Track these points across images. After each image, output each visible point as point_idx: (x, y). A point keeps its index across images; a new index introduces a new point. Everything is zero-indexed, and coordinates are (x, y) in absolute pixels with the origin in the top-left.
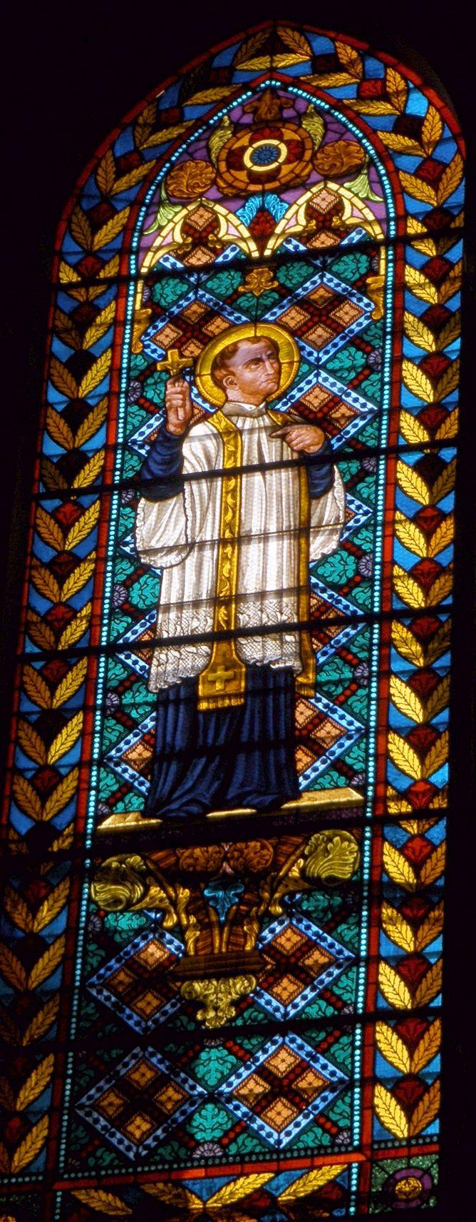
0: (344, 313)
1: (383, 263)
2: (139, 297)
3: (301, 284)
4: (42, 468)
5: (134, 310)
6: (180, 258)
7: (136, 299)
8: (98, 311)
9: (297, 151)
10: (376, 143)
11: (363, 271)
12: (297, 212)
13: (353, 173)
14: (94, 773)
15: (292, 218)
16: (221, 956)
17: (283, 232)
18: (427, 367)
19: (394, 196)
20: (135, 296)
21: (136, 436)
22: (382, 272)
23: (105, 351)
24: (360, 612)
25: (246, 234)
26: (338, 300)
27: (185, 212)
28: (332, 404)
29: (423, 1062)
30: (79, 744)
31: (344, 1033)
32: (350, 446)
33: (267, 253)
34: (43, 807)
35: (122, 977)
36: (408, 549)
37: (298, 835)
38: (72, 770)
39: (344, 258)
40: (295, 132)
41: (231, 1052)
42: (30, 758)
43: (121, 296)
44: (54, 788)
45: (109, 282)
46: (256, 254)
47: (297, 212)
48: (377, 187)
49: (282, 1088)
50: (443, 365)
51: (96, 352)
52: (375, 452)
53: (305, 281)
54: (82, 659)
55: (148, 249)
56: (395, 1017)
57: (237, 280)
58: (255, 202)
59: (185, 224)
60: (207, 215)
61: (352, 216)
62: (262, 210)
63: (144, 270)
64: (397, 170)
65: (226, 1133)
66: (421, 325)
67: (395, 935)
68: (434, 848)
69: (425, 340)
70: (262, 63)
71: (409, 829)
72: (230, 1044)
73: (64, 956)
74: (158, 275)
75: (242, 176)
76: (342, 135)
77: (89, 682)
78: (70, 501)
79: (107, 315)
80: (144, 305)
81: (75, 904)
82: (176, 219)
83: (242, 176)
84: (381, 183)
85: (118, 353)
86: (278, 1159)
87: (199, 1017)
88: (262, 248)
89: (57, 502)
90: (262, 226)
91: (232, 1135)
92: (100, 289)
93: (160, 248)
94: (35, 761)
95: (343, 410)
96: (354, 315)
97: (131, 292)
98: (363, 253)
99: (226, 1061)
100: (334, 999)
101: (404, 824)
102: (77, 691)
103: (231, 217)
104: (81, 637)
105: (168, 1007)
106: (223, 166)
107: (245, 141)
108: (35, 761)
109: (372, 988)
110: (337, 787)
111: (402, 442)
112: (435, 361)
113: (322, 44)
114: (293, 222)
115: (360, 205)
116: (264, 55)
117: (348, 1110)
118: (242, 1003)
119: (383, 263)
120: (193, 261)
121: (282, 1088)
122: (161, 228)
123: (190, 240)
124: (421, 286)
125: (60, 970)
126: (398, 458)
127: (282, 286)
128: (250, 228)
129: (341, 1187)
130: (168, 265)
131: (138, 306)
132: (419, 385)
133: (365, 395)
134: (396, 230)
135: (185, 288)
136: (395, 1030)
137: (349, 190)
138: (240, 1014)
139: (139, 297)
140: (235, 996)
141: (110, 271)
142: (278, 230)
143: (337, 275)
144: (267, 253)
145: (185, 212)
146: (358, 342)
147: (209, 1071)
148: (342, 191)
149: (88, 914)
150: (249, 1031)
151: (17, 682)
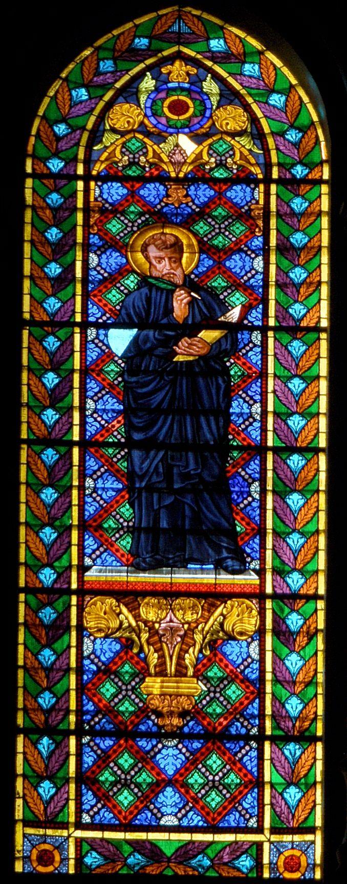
33: (181, 175)
39: (234, 187)
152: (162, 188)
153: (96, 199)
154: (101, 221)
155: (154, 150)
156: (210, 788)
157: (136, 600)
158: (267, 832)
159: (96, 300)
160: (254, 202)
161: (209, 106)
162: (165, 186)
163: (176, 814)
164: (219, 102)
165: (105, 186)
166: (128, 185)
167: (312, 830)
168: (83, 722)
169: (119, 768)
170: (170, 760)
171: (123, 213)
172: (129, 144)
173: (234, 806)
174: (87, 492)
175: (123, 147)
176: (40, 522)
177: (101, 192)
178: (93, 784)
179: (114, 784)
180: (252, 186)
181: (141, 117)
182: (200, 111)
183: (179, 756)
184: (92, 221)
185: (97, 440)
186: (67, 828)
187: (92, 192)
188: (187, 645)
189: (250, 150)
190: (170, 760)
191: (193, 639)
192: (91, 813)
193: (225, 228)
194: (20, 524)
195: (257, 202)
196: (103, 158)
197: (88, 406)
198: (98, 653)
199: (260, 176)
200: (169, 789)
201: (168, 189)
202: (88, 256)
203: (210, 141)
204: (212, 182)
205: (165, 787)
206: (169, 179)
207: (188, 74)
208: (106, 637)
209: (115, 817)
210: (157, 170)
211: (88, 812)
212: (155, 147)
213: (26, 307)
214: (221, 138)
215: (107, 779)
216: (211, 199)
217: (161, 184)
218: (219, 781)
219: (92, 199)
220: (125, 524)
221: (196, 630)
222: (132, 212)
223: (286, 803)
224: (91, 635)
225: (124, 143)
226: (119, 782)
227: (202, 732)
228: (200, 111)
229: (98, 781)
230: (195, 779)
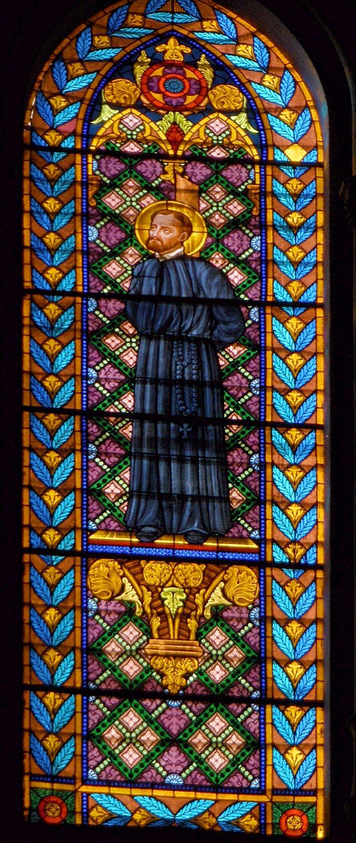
17: (190, 141)
24: (252, 419)
25: (164, 138)
27: (120, 115)
33: (179, 153)
34: (52, 477)
38: (70, 379)
39: (230, 167)
42: (40, 597)
46: (171, 152)
55: (95, 136)
61: (237, 139)
82: (114, 119)
94: (43, 600)
108: (43, 600)
114: (195, 136)
115: (243, 134)
122: (103, 123)
128: (167, 135)
135: (123, 166)
137: (234, 121)
144: (179, 153)
145: (120, 115)
148: (229, 121)
152: (158, 164)
153: (94, 173)
154: (99, 195)
155: (151, 128)
156: (214, 749)
157: (139, 565)
158: (269, 793)
159: (96, 344)
160: (250, 182)
161: (204, 85)
162: (162, 163)
163: (180, 774)
164: (214, 79)
165: (103, 161)
166: (127, 161)
167: (314, 792)
168: (88, 680)
169: (124, 727)
170: (174, 720)
171: (121, 187)
172: (126, 120)
173: (237, 768)
174: (90, 614)
175: (120, 123)
176: (42, 525)
177: (99, 166)
178: (99, 495)
179: (120, 655)
180: (249, 167)
181: (138, 92)
182: (196, 90)
183: (183, 716)
184: (91, 193)
185: (99, 409)
186: (74, 784)
187: (90, 166)
188: (189, 609)
189: (246, 130)
190: (174, 720)
191: (194, 603)
192: (97, 443)
193: (223, 206)
194: (23, 526)
195: (254, 183)
196: (100, 133)
197: (90, 606)
198: (104, 170)
199: (257, 158)
200: (174, 749)
201: (164, 166)
202: (87, 230)
203: (206, 120)
204: (208, 161)
205: (170, 746)
206: (166, 156)
207: (182, 52)
208: (112, 599)
209: (121, 774)
210: (155, 147)
211: (94, 769)
212: (152, 124)
213: (27, 276)
214: (218, 117)
215: (113, 650)
216: (208, 178)
217: (158, 160)
218: (222, 742)
219: (90, 173)
220: (128, 648)
221: (197, 595)
222: (131, 187)
223: (288, 764)
224: (94, 596)
225: (121, 119)
226: (125, 652)
227: (205, 693)
228: (196, 90)
229: (104, 493)
230: (199, 739)
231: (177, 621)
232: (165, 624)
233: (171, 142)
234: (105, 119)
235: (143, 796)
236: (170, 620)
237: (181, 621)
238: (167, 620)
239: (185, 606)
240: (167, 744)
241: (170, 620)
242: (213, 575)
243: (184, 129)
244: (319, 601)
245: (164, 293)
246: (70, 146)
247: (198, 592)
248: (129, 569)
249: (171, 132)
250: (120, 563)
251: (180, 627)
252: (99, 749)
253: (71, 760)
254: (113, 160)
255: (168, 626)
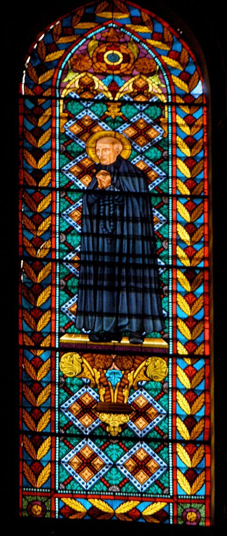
0: (151, 133)
1: (166, 113)
2: (61, 107)
3: (132, 117)
4: (22, 313)
5: (59, 113)
6: (79, 94)
7: (59, 111)
8: (44, 111)
9: (127, 58)
10: (162, 61)
11: (158, 115)
12: (129, 85)
13: (151, 74)
14: (58, 266)
15: (127, 86)
16: (114, 404)
18: (188, 476)
19: (170, 85)
20: (59, 106)
21: (64, 168)
22: (166, 116)
23: (48, 129)
25: (107, 89)
26: (149, 127)
28: (148, 406)
29: (196, 411)
30: (50, 452)
31: (165, 446)
32: (156, 190)
33: (116, 99)
34: (37, 374)
35: (74, 406)
36: (183, 311)
37: (143, 357)
40: (126, 49)
41: (121, 447)
43: (53, 106)
44: (41, 472)
45: (47, 98)
46: (111, 99)
47: (129, 85)
48: (163, 81)
49: (141, 466)
50: (194, 229)
51: (45, 128)
52: (167, 195)
53: (134, 116)
54: (48, 262)
55: (64, 88)
56: (183, 442)
57: (105, 109)
58: (110, 78)
59: (79, 81)
60: (89, 80)
62: (113, 81)
63: (63, 96)
64: (171, 75)
65: (121, 482)
66: (184, 144)
67: (183, 150)
68: (197, 372)
69: (187, 152)
70: (109, 15)
71: (187, 362)
72: (121, 444)
73: (50, 473)
74: (68, 99)
75: (104, 65)
76: (146, 55)
77: (52, 273)
78: (38, 191)
79: (48, 112)
80: (64, 112)
81: (53, 449)
82: (76, 78)
83: (104, 65)
84: (164, 79)
85: (53, 361)
86: (143, 497)
87: (107, 430)
88: (114, 96)
89: (33, 191)
90: (114, 88)
91: (123, 483)
92: (43, 100)
93: (69, 89)
95: (153, 410)
96: (155, 133)
97: (58, 105)
98: (158, 106)
99: (119, 451)
100: (160, 431)
101: (186, 360)
102: (47, 481)
103: (100, 82)
104: (47, 207)
105: (94, 423)
106: (95, 60)
107: (103, 50)
109: (174, 429)
110: (156, 338)
111: (178, 193)
112: (191, 227)
113: (135, 12)
116: (109, 11)
117: (167, 479)
118: (124, 426)
119: (166, 113)
120: (84, 96)
121: (141, 466)
122: (69, 81)
123: (82, 87)
124: (182, 125)
125: (49, 425)
126: (177, 200)
127: (124, 115)
129: (166, 512)
130: (73, 96)
131: (61, 111)
132: (184, 170)
133: (162, 169)
134: (172, 262)
136: (184, 448)
138: (123, 431)
139: (61, 107)
140: (121, 423)
141: (48, 93)
142: (121, 90)
143: (147, 115)
144: (116, 99)
145: (79, 76)
146: (157, 145)
147: (113, 454)
148: (148, 80)
149: (59, 377)
150: (127, 439)
151: (21, 391)
170: (114, 452)
231: (116, 391)
232: (108, 392)
233: (111, 92)
234: (71, 79)
235: (89, 370)
236: (112, 391)
237: (119, 390)
238: (109, 390)
239: (121, 381)
240: (110, 467)
241: (112, 391)
242: (137, 366)
243: (120, 85)
244: (207, 483)
245: (116, 294)
246: (48, 95)
247: (130, 372)
248: (86, 358)
249: (111, 86)
250: (80, 355)
251: (118, 395)
252: (66, 470)
253: (48, 451)
254: (76, 104)
255: (110, 394)
